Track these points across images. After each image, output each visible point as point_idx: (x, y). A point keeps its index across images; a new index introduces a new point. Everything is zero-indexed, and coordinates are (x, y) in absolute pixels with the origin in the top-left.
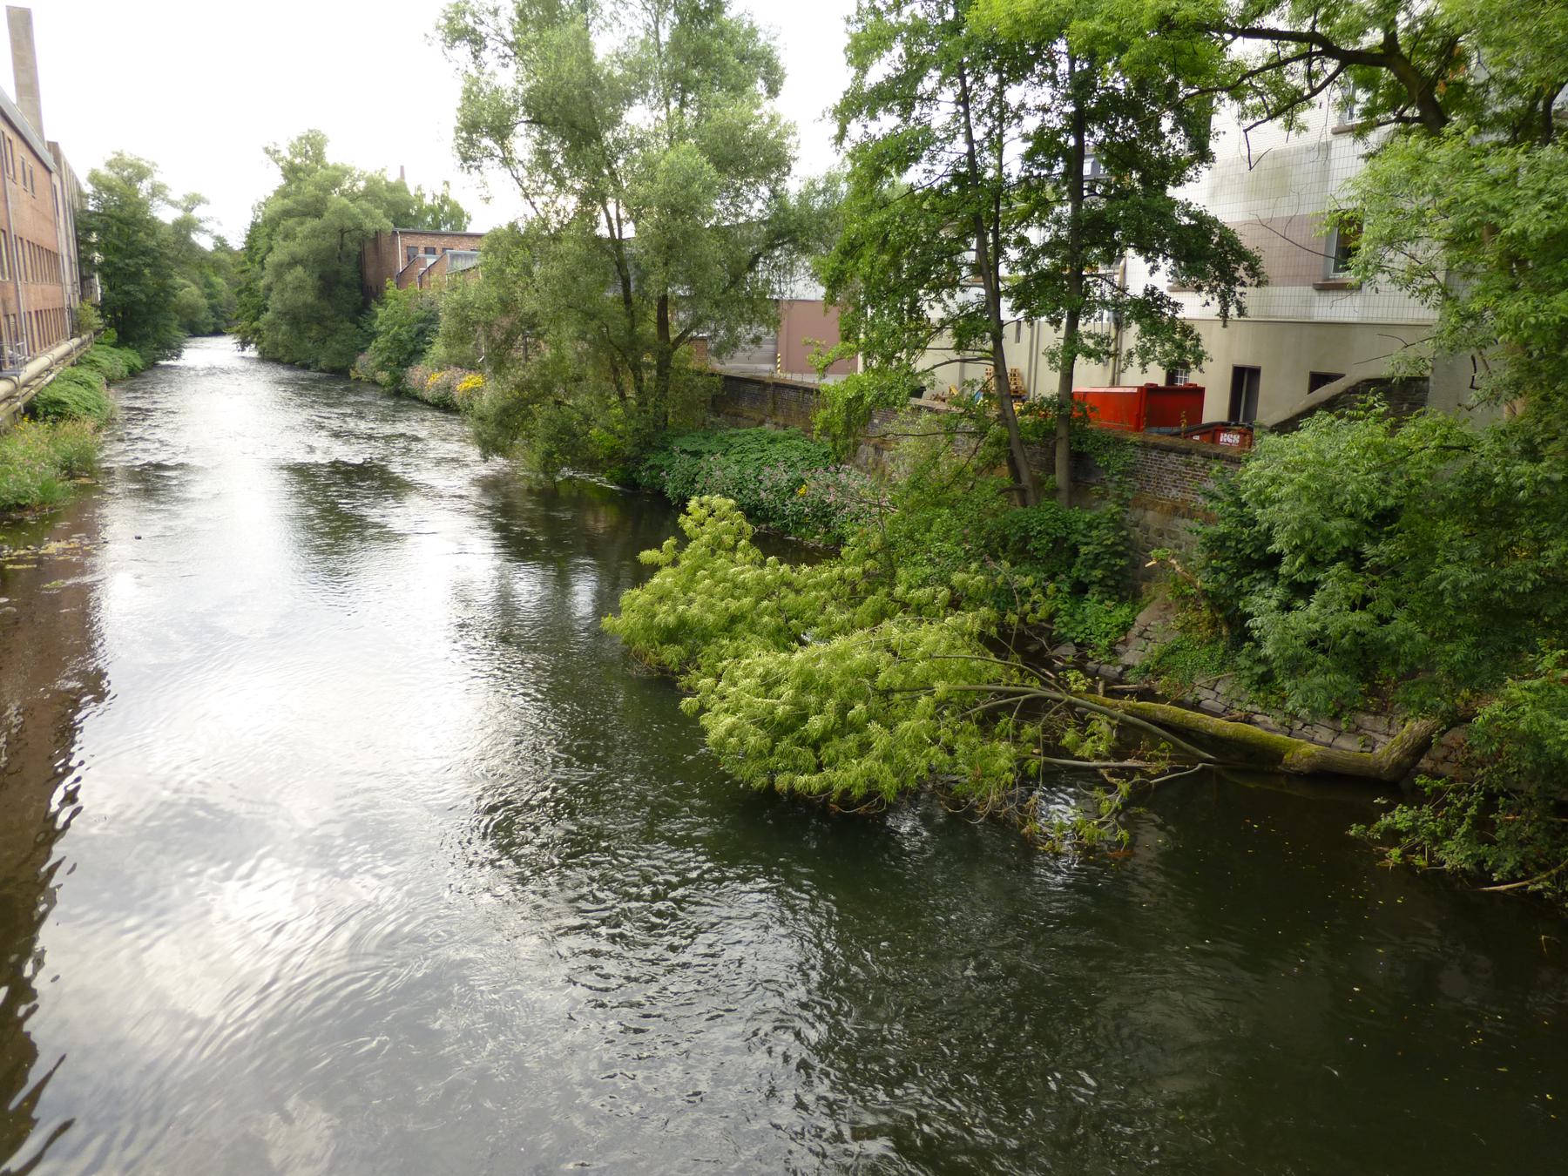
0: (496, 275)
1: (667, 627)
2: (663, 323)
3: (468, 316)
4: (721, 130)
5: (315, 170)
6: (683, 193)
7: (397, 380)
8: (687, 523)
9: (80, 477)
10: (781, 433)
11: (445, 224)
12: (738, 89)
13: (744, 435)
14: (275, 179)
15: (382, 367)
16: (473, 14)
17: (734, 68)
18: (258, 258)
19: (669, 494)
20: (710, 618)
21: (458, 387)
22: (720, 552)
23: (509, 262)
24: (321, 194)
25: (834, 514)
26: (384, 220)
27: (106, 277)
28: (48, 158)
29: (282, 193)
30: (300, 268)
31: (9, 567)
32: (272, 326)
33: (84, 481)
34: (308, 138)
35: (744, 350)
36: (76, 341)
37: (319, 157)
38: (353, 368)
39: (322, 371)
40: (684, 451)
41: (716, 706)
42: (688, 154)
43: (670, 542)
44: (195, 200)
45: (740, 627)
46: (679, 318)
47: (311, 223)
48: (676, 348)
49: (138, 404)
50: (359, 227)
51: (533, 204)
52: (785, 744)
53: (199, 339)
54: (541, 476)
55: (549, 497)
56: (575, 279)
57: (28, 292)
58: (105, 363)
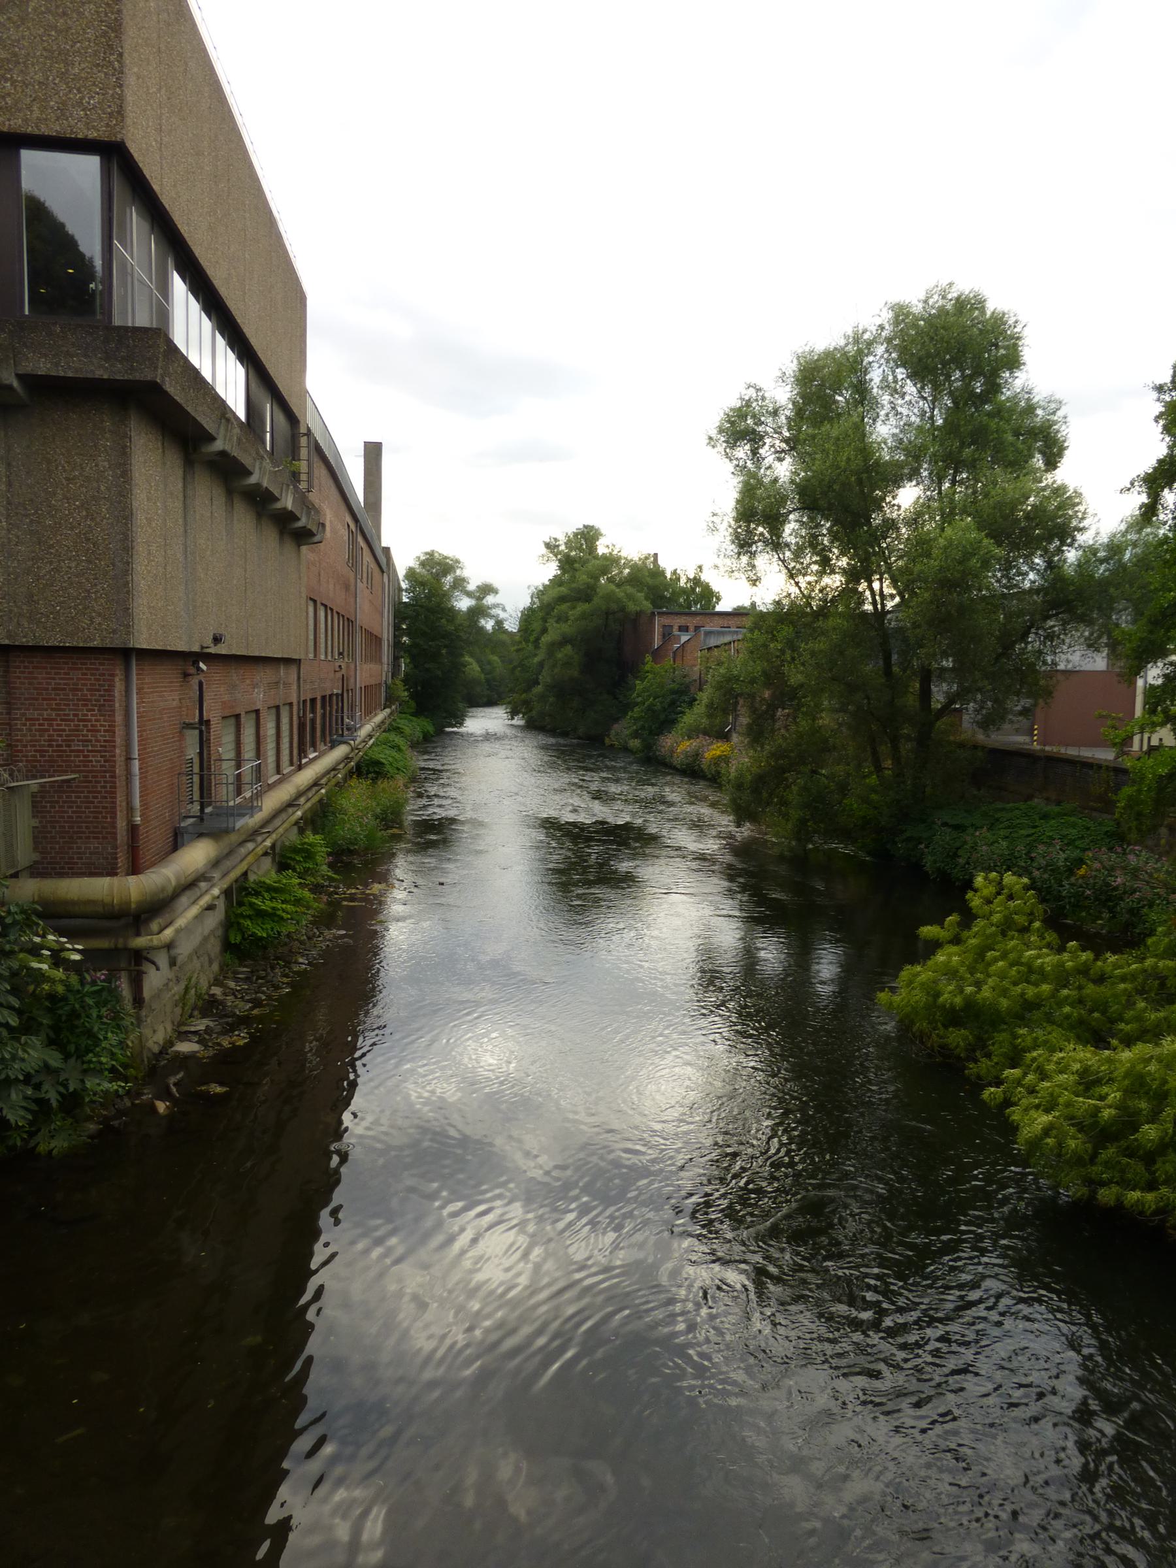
0: (757, 652)
1: (952, 1008)
2: (926, 694)
3: (732, 689)
4: (999, 506)
5: (587, 561)
6: (960, 568)
7: (648, 747)
8: (975, 901)
9: (392, 827)
10: (1056, 809)
11: (696, 604)
12: (1017, 464)
13: (1012, 810)
14: (551, 570)
15: (635, 735)
16: (754, 416)
17: (1012, 444)
18: (532, 638)
19: (928, 867)
20: (1004, 1003)
21: (706, 755)
22: (1010, 933)
23: (774, 639)
24: (591, 581)
25: (1121, 899)
26: (645, 602)
27: (413, 658)
28: (383, 561)
29: (556, 582)
30: (569, 647)
31: (345, 903)
32: (542, 698)
33: (396, 831)
34: (582, 533)
35: (1012, 722)
36: (388, 711)
37: (592, 549)
38: (608, 736)
39: (579, 738)
40: (945, 824)
41: (1024, 1101)
42: (965, 528)
43: (952, 919)
44: (487, 590)
45: (1037, 1015)
46: (939, 694)
47: (582, 607)
48: (938, 719)
49: (431, 765)
50: (623, 609)
51: (797, 584)
52: (1109, 1152)
53: (474, 709)
54: (794, 843)
55: (800, 862)
56: (841, 653)
57: (361, 670)
58: (407, 731)
